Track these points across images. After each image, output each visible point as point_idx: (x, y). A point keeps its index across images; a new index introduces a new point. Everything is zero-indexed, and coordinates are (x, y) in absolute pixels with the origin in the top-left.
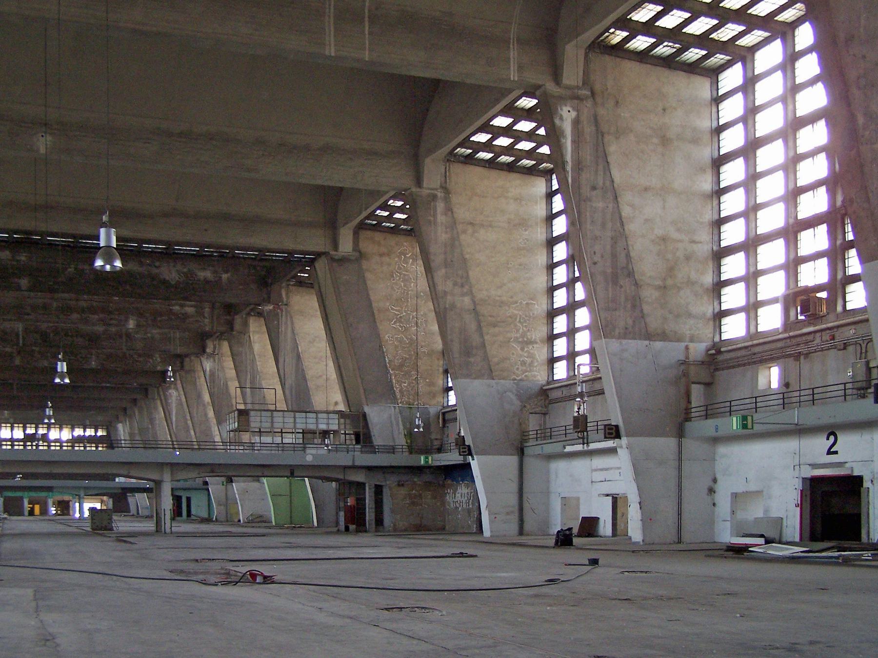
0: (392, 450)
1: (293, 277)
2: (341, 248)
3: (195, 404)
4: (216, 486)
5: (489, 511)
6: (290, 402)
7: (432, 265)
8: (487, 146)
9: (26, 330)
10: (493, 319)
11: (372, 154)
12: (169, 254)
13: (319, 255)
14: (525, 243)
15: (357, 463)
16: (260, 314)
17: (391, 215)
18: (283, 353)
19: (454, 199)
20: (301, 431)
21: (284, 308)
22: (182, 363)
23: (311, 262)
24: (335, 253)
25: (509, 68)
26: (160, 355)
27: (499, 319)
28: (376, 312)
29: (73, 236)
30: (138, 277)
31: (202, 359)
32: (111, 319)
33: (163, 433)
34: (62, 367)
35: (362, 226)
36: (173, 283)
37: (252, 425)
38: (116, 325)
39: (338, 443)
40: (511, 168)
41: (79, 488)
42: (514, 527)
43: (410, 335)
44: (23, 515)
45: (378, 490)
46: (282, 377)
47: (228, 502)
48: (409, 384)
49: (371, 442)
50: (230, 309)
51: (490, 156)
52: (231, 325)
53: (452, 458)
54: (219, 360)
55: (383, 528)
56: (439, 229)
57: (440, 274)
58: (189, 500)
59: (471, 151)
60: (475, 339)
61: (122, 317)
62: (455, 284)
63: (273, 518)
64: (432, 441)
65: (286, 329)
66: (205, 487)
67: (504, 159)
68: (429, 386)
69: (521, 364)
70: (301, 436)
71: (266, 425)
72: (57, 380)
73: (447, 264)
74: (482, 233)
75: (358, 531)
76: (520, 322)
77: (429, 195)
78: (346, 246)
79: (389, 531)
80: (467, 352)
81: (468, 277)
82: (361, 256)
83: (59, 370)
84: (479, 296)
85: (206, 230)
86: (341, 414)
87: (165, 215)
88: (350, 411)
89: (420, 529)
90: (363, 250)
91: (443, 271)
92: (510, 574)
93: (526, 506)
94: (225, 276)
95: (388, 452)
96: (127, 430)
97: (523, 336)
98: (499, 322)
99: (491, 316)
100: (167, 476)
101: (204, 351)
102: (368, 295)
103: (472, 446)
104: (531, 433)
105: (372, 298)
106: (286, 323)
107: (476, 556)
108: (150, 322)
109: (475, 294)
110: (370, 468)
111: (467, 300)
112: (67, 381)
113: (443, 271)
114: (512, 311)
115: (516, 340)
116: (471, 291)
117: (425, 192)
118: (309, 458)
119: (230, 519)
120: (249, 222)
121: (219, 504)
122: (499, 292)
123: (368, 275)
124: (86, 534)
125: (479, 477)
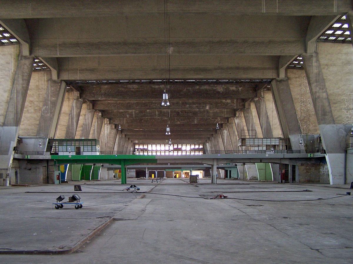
0: (299, 152)
1: (265, 88)
2: (280, 77)
3: (233, 136)
4: (239, 166)
5: (332, 175)
6: (264, 134)
7: (311, 82)
8: (333, 35)
9: (171, 112)
10: (335, 101)
11: (288, 42)
12: (218, 82)
13: (272, 79)
14: (349, 71)
15: (285, 157)
16: (254, 102)
17: (299, 63)
18: (262, 116)
19: (320, 56)
20: (265, 145)
21: (262, 99)
22: (228, 120)
23: (270, 82)
24: (278, 78)
25: (334, 7)
26: (220, 118)
27: (337, 101)
28: (294, 99)
29: (184, 79)
30: (208, 91)
31: (235, 119)
32: (200, 106)
33: (222, 148)
34: (168, 129)
35: (288, 68)
36: (221, 92)
37: (247, 144)
38: (203, 108)
39: (278, 150)
40: (343, 42)
41: (191, 168)
42: (342, 181)
43: (307, 107)
44: (173, 178)
45: (294, 167)
46: (261, 125)
47: (244, 172)
48: (306, 126)
49: (291, 149)
50: (244, 100)
51: (334, 38)
52: (244, 106)
53: (319, 155)
54: (241, 119)
55: (296, 181)
56: (314, 68)
57: (313, 86)
58: (230, 171)
59: (326, 37)
60: (328, 109)
61: (204, 105)
62: (320, 88)
63: (259, 178)
64: (315, 148)
65: (263, 106)
66: (236, 166)
67: (340, 39)
68: (315, 127)
69: (347, 118)
70: (265, 147)
71: (260, 144)
72: (167, 134)
73: (316, 81)
74: (331, 68)
75: (285, 183)
76: (346, 101)
77: (310, 55)
78: (282, 75)
79: (298, 182)
80: (324, 114)
81: (325, 86)
82: (288, 79)
83: (167, 130)
84: (329, 92)
85: (230, 74)
86: (280, 139)
87: (215, 69)
88: (284, 137)
89: (309, 181)
90: (289, 77)
91: (315, 84)
92: (310, 197)
93: (347, 173)
94: (240, 89)
95: (298, 153)
96: (210, 145)
97: (347, 107)
98: (337, 102)
99: (334, 100)
100: (215, 163)
101: (235, 116)
102: (291, 93)
103: (326, 149)
104: (350, 144)
105: (292, 94)
106: (263, 104)
107: (312, 191)
108: (214, 106)
109: (328, 92)
110: (290, 159)
111: (324, 94)
112: (170, 134)
113: (315, 84)
114: (343, 97)
115: (345, 109)
116: (326, 91)
117: (308, 54)
118: (267, 155)
119: (244, 179)
120: (246, 69)
121: (241, 173)
122: (338, 91)
123: (291, 86)
124: (188, 184)
125: (329, 162)
